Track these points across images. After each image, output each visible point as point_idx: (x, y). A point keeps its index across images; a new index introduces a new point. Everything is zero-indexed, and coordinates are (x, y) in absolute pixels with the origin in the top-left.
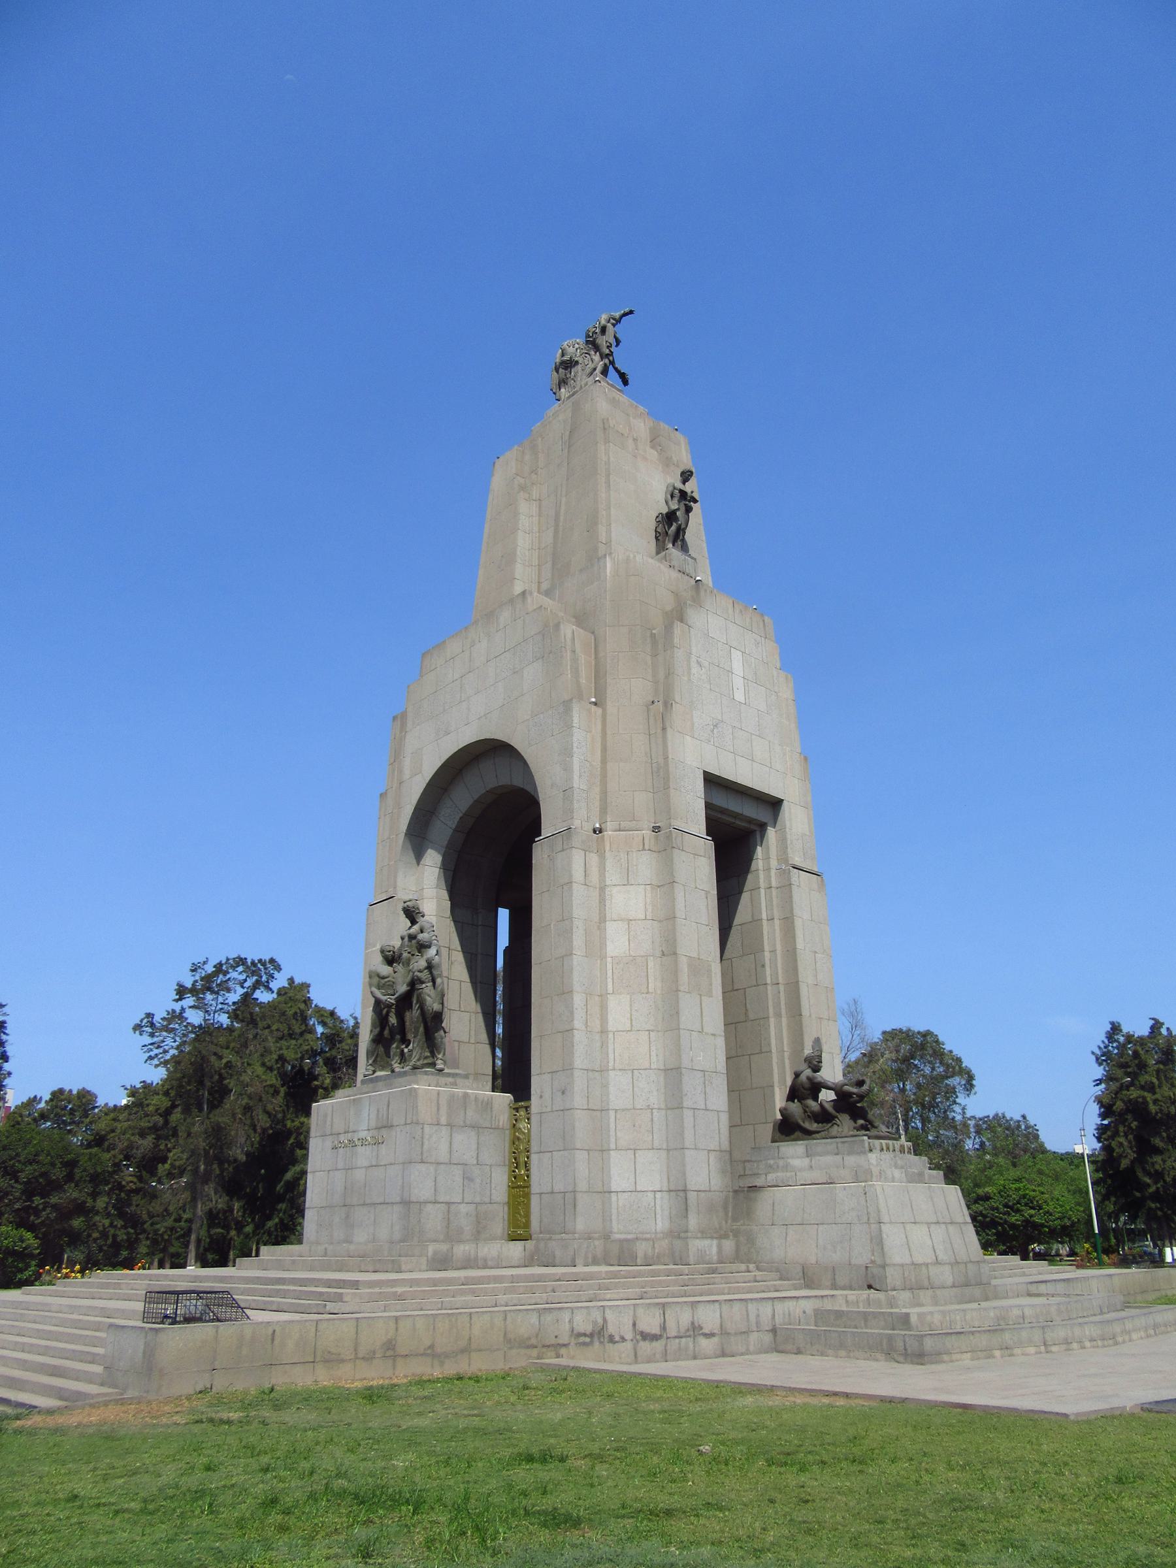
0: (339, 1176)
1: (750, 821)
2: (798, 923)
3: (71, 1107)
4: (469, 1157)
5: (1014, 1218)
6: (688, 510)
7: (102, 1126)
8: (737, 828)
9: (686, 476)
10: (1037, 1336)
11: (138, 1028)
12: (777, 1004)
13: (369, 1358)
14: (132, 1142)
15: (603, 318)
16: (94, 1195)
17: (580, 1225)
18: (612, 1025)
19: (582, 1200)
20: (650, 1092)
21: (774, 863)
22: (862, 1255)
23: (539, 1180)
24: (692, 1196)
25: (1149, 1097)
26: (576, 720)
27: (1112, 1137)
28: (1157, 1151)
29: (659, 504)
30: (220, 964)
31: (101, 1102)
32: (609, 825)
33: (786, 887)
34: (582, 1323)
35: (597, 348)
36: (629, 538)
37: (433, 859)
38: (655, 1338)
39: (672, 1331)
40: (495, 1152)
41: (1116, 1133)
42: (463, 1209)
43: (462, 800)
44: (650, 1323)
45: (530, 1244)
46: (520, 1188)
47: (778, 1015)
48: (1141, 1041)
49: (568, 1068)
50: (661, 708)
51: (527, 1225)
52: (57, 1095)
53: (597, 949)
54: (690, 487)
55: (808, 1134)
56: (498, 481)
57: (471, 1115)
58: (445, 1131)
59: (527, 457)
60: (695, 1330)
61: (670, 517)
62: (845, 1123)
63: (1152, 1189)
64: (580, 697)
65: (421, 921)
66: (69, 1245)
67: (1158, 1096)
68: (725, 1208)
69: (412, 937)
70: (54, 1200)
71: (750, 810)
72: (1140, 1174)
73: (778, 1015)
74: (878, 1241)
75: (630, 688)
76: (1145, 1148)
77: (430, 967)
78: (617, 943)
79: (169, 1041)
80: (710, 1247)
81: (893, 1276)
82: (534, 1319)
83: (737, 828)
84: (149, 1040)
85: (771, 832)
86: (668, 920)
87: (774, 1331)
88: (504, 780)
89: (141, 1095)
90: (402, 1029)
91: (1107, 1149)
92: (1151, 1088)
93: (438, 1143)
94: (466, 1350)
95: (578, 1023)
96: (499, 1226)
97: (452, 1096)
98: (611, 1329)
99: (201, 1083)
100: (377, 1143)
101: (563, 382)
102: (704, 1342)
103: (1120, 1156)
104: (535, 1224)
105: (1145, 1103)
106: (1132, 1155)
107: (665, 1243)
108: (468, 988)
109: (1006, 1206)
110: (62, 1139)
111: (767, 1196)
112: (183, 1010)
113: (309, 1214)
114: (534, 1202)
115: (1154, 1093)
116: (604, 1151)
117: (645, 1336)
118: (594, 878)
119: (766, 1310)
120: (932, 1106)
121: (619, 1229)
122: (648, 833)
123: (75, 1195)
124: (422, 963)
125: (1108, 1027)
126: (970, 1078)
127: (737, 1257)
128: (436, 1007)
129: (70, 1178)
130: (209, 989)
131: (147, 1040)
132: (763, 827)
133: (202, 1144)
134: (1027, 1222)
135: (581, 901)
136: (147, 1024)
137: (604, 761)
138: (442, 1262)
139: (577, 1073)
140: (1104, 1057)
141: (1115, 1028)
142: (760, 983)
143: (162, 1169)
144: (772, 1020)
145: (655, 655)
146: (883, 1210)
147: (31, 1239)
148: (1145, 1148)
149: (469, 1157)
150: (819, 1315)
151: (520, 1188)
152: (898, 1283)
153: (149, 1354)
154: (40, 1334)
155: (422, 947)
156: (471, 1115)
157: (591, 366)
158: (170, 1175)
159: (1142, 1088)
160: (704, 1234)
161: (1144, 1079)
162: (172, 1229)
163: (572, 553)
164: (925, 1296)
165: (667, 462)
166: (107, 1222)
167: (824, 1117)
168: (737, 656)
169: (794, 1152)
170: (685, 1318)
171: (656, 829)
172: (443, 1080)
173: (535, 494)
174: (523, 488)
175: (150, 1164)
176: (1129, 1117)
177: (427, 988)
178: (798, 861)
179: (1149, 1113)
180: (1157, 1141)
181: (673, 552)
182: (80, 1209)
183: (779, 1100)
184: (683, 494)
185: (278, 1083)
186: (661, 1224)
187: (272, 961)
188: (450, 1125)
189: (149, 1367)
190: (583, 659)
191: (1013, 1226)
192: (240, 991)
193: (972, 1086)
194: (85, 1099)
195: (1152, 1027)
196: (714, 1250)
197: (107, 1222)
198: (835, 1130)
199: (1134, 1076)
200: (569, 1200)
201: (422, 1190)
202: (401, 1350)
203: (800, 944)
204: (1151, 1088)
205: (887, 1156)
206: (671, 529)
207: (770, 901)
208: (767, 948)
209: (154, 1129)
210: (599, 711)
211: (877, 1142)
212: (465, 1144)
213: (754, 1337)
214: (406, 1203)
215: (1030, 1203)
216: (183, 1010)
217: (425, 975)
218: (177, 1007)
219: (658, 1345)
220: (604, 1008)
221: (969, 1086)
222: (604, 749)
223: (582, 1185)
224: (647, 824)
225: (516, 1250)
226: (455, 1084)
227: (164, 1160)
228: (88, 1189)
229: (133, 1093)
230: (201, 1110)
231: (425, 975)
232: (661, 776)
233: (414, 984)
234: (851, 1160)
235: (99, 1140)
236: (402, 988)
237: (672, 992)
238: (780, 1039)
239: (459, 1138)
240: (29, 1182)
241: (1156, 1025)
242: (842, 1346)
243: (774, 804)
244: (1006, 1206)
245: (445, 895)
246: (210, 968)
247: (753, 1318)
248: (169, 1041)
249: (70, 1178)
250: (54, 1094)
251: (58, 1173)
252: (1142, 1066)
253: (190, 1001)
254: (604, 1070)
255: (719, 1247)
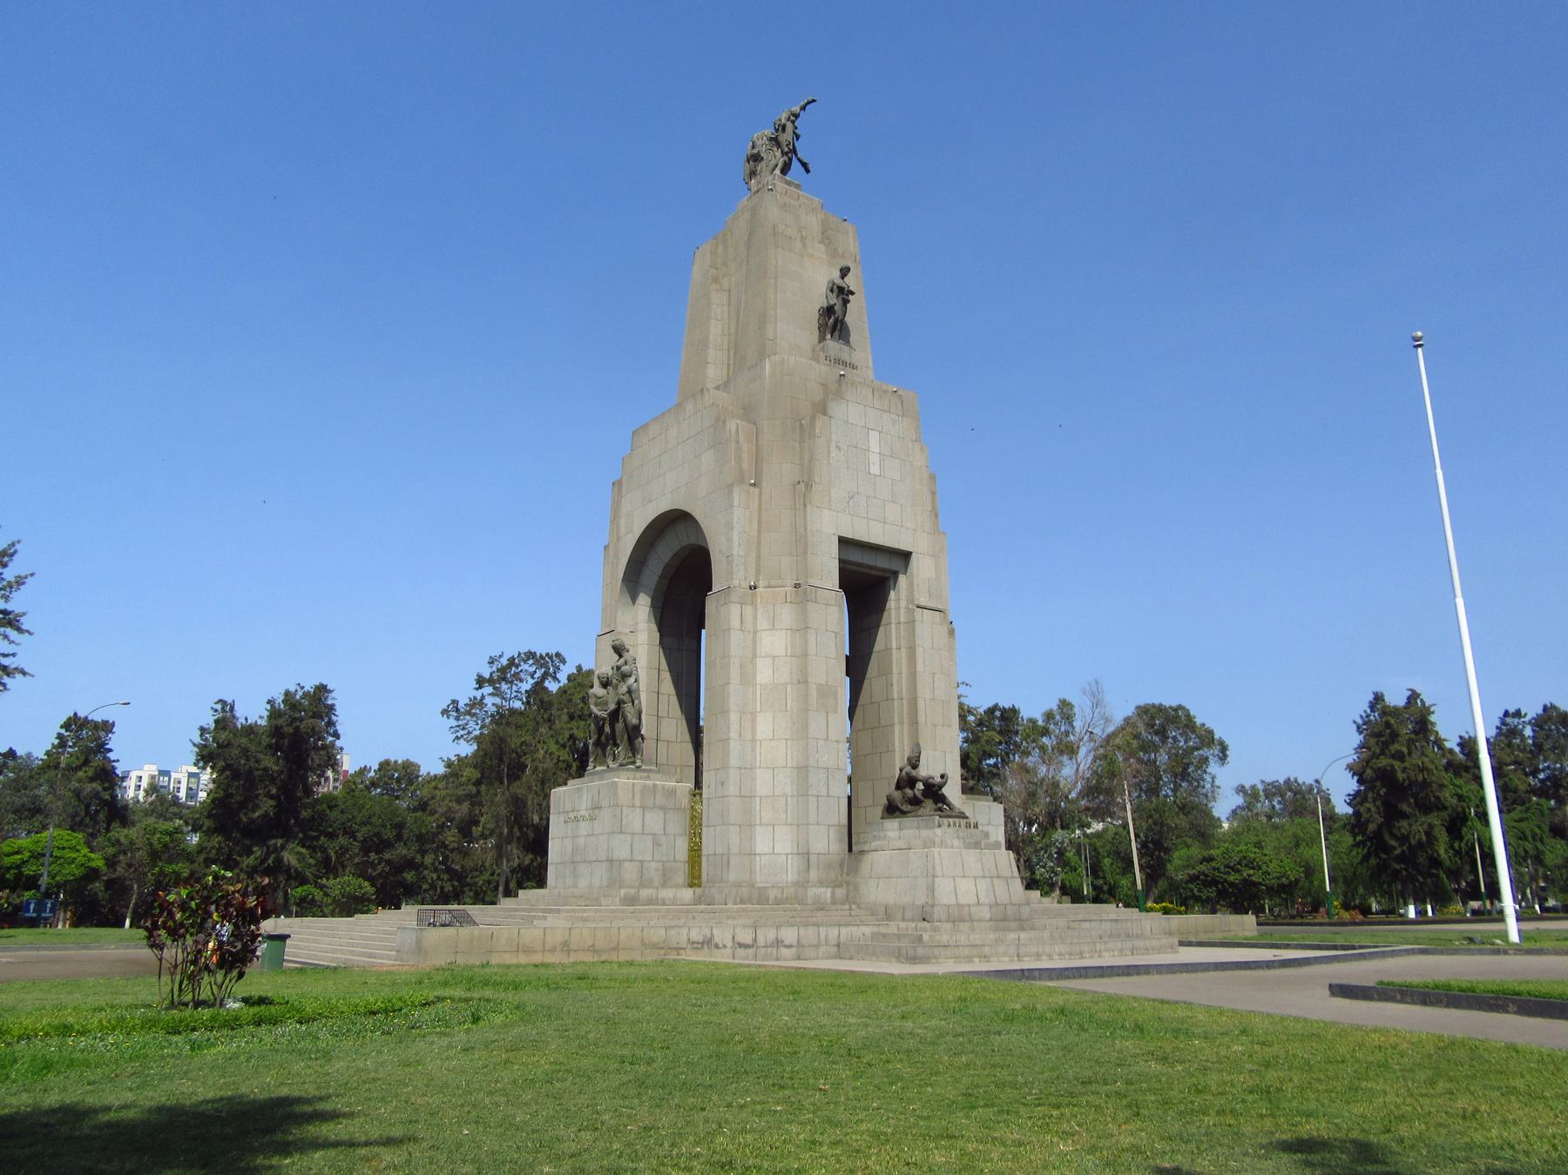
0: (568, 843)
1: (884, 570)
2: (919, 651)
3: (397, 776)
4: (658, 828)
5: (1232, 878)
6: (846, 302)
7: (424, 793)
8: (867, 582)
9: (844, 272)
10: (1012, 950)
11: (445, 712)
12: (901, 716)
13: (553, 951)
14: (449, 809)
15: (784, 116)
16: (423, 852)
17: (732, 877)
18: (759, 736)
19: (734, 860)
20: (786, 784)
21: (903, 603)
22: (921, 899)
23: (707, 848)
24: (813, 858)
25: (1397, 764)
26: (736, 503)
27: (1361, 803)
28: (1405, 816)
29: (819, 297)
30: (513, 659)
31: (423, 772)
32: (761, 584)
33: (911, 622)
34: (696, 935)
35: (779, 145)
36: (794, 328)
37: (644, 601)
38: (747, 946)
39: (761, 941)
40: (677, 826)
41: (1365, 799)
42: (653, 865)
43: (664, 554)
44: (745, 936)
45: (698, 890)
46: (695, 852)
47: (902, 723)
48: (1395, 712)
49: (725, 767)
50: (804, 487)
51: (699, 877)
52: (384, 765)
53: (748, 678)
54: (851, 282)
55: (904, 813)
56: (697, 272)
57: (659, 800)
58: (638, 811)
59: (720, 249)
60: (778, 943)
61: (829, 310)
62: (929, 805)
63: (1398, 851)
64: (742, 481)
65: (626, 655)
66: (405, 894)
67: (1407, 764)
68: (841, 866)
69: (618, 668)
70: (387, 856)
71: (883, 563)
72: (1387, 837)
73: (902, 723)
74: (931, 889)
75: (780, 471)
76: (1392, 813)
77: (630, 692)
78: (764, 674)
79: (472, 724)
80: (826, 893)
81: (938, 912)
82: (662, 932)
83: (867, 582)
84: (455, 723)
85: (902, 579)
86: (802, 656)
87: (838, 945)
88: (685, 542)
89: (455, 768)
90: (613, 736)
91: (1357, 814)
92: (1400, 757)
93: (634, 819)
94: (616, 949)
95: (733, 734)
96: (681, 876)
97: (645, 786)
98: (717, 939)
99: (501, 760)
100: (592, 819)
101: (753, 174)
102: (784, 951)
103: (1368, 821)
104: (704, 876)
105: (1393, 771)
106: (1381, 820)
107: (792, 890)
108: (674, 699)
109: (1227, 866)
110: (390, 805)
111: (869, 858)
112: (483, 697)
113: (550, 868)
114: (704, 859)
115: (1403, 761)
116: (751, 826)
117: (741, 945)
118: (749, 625)
119: (833, 932)
120: (1184, 775)
121: (760, 881)
122: (790, 589)
123: (404, 852)
124: (624, 689)
125: (1371, 697)
126: (1224, 749)
127: (848, 900)
128: (635, 721)
129: (399, 837)
130: (504, 679)
131: (453, 722)
132: (895, 574)
133: (504, 811)
134: (1245, 880)
135: (737, 643)
136: (452, 710)
137: (759, 532)
138: (631, 901)
139: (732, 771)
140: (1364, 727)
141: (1378, 698)
142: (889, 699)
143: (476, 831)
144: (897, 728)
145: (802, 442)
146: (938, 868)
147: (367, 887)
148: (1392, 813)
149: (658, 828)
150: (874, 936)
151: (695, 852)
152: (943, 918)
153: (419, 942)
154: (364, 938)
155: (625, 676)
156: (659, 800)
157: (773, 162)
158: (484, 837)
159: (1393, 757)
160: (821, 883)
161: (1394, 747)
162: (489, 882)
163: (747, 351)
164: (964, 927)
165: (833, 253)
166: (435, 876)
167: (915, 802)
168: (874, 436)
169: (892, 825)
170: (771, 935)
171: (797, 586)
172: (638, 774)
173: (726, 286)
174: (715, 280)
175: (466, 828)
176: (1378, 784)
177: (628, 708)
178: (923, 601)
179: (1397, 780)
180: (1405, 807)
181: (832, 345)
182: (410, 864)
183: (890, 788)
184: (841, 290)
185: (570, 759)
186: (791, 876)
187: (558, 655)
188: (643, 807)
189: (419, 949)
190: (745, 446)
191: (1232, 885)
192: (531, 681)
193: (1225, 756)
194: (408, 771)
195: (1409, 698)
196: (829, 895)
197: (435, 876)
198: (921, 811)
199: (1385, 745)
200: (725, 860)
201: (621, 852)
202: (573, 947)
203: (920, 667)
204: (1400, 757)
205: (952, 830)
206: (833, 323)
207: (898, 633)
208: (895, 671)
209: (469, 796)
210: (757, 490)
211: (946, 821)
212: (654, 820)
213: (822, 949)
214: (610, 861)
215: (1251, 864)
216: (483, 697)
217: (626, 698)
218: (478, 694)
219: (750, 951)
220: (754, 722)
221: (1223, 757)
222: (760, 522)
223: (735, 850)
224: (790, 582)
225: (688, 894)
226: (648, 778)
227: (477, 823)
228: (416, 847)
229: (449, 764)
230: (502, 783)
231: (626, 698)
232: (801, 544)
233: (620, 703)
234: (924, 833)
235: (423, 806)
236: (612, 706)
237: (805, 709)
238: (902, 742)
239: (648, 815)
240: (365, 840)
241: (1413, 696)
242: (874, 954)
243: (906, 556)
244: (1227, 866)
245: (655, 628)
246: (504, 661)
247: (822, 937)
248: (472, 724)
249: (399, 837)
250: (381, 765)
251: (389, 834)
252: (1395, 736)
253: (488, 689)
254: (752, 768)
255: (833, 893)
